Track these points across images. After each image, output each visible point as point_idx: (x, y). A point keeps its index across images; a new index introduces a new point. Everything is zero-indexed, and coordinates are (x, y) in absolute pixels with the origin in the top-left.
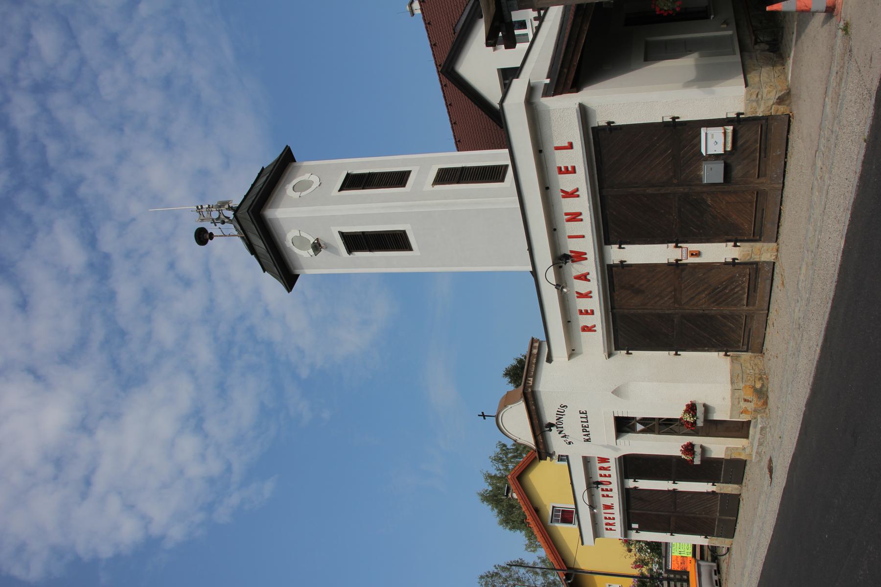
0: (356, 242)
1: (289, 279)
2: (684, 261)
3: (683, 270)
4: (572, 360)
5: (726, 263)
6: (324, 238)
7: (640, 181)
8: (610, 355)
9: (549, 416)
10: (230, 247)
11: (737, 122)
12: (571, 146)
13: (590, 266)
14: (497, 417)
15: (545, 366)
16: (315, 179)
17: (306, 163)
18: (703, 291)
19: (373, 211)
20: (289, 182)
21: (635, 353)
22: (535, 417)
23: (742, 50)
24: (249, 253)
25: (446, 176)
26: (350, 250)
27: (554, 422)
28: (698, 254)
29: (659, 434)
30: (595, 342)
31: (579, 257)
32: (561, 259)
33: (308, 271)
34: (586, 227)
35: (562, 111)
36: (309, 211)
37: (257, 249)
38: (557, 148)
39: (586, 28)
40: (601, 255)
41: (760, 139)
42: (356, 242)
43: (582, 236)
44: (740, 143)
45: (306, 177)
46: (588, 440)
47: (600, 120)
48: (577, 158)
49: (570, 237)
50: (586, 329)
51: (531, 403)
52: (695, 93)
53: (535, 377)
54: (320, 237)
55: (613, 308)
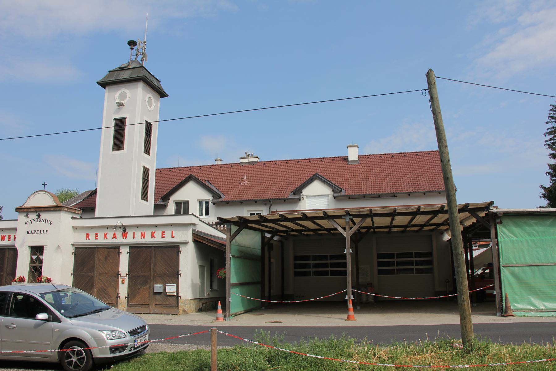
0: (120, 125)
1: (104, 84)
2: (120, 277)
3: (115, 277)
4: (72, 228)
5: (118, 294)
6: (124, 108)
7: (154, 263)
8: (73, 245)
9: (44, 216)
10: (125, 57)
11: (177, 297)
12: (173, 237)
13: (119, 239)
14: (44, 191)
15: (70, 216)
16: (152, 109)
17: (159, 103)
18: (105, 285)
19: (134, 136)
20: (152, 96)
21: (73, 257)
22: (46, 209)
23: (201, 299)
24: (119, 66)
25: (146, 172)
26: (116, 120)
27: (41, 217)
28: (123, 283)
29: (30, 266)
30: (81, 239)
31: (125, 236)
32: (124, 229)
33: (106, 95)
34: (138, 240)
35: (187, 235)
36: (137, 103)
37: (122, 73)
38: (172, 232)
39: (215, 246)
40: (124, 245)
41: (172, 303)
42: (120, 125)
43: (135, 238)
44: (169, 297)
45: (154, 104)
46: (28, 232)
47: (182, 248)
48: (168, 239)
49: (134, 233)
50: (88, 236)
51: (55, 209)
52: (189, 282)
53: (67, 211)
54: (97, 81)
55: (98, 248)
